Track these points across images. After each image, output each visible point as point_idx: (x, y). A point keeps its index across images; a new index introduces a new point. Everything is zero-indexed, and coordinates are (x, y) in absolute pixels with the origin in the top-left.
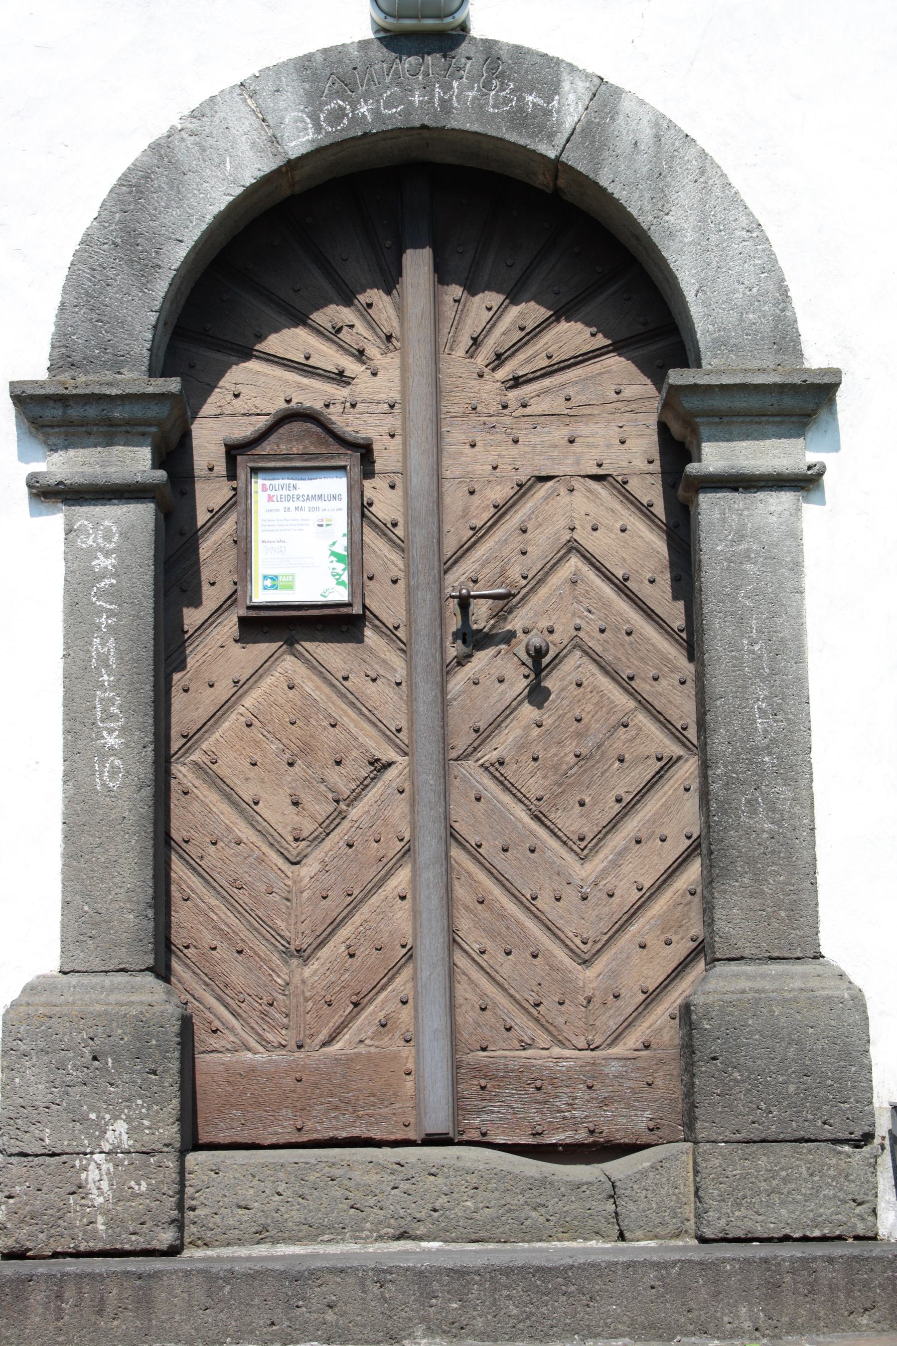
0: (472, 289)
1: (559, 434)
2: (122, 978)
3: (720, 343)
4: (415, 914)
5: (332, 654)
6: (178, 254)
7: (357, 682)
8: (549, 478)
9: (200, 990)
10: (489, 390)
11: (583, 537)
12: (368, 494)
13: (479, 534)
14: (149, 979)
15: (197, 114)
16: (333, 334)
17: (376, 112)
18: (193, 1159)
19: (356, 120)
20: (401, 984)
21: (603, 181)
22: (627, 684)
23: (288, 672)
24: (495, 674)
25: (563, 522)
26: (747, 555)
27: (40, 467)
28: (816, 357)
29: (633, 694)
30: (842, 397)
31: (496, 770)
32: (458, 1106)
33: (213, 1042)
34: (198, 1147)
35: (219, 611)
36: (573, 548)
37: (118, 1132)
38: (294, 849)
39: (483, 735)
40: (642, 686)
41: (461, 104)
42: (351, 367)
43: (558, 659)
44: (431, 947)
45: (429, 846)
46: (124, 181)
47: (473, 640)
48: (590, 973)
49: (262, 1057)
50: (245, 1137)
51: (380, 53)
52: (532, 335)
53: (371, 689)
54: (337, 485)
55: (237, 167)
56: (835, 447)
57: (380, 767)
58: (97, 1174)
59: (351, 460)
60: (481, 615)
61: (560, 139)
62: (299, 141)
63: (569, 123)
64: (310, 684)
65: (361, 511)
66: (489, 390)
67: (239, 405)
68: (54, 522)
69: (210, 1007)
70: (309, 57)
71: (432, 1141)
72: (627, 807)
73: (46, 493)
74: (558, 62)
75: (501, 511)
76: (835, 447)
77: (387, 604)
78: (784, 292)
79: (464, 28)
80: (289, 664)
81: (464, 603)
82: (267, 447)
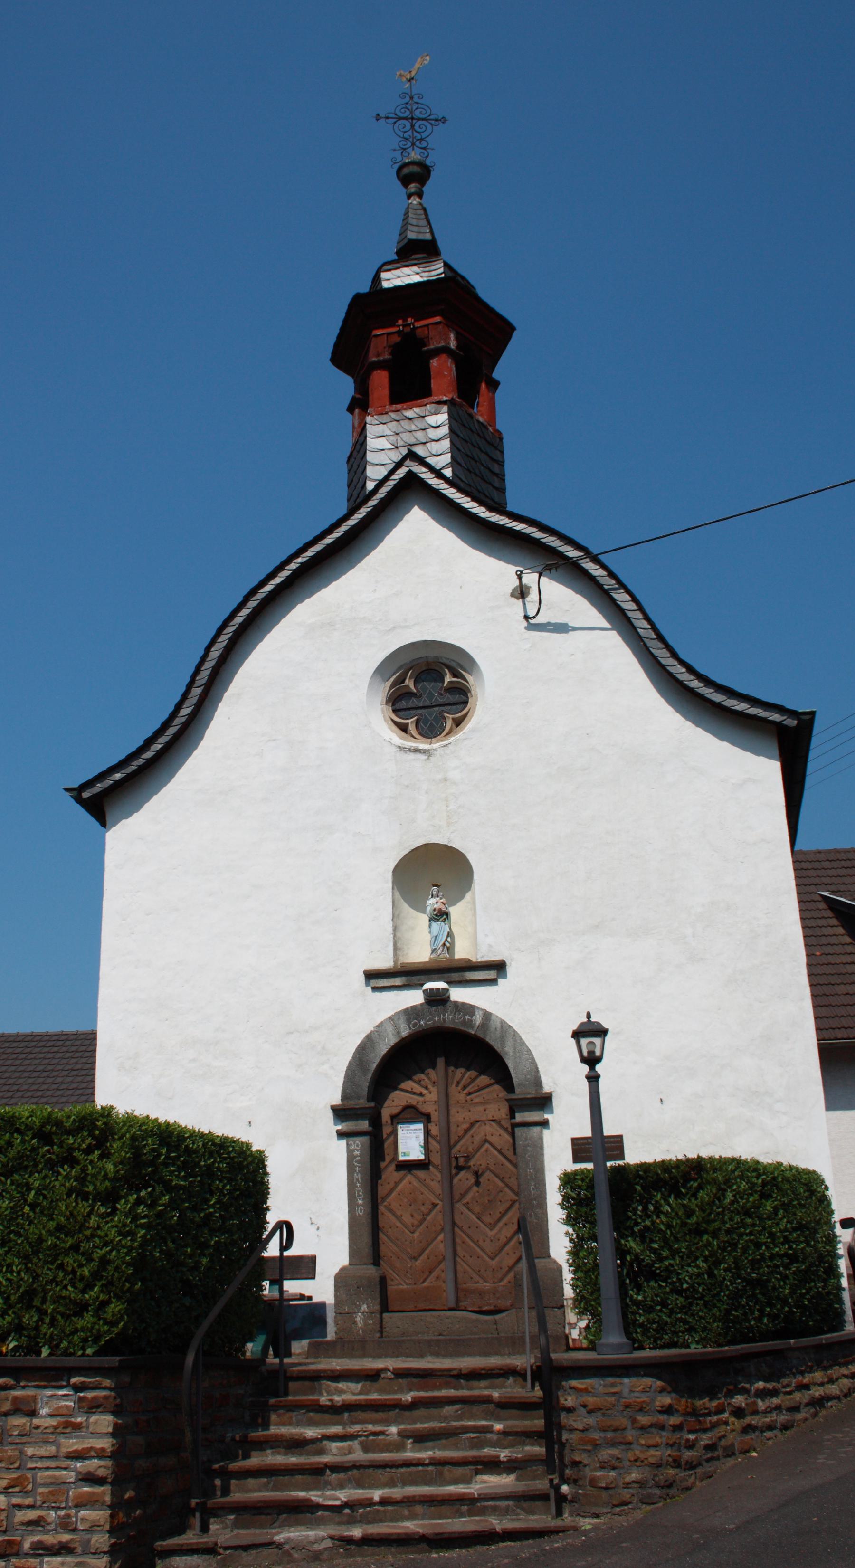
0: (457, 1067)
1: (481, 1108)
2: (365, 1266)
3: (519, 1085)
4: (445, 1246)
5: (421, 1174)
6: (374, 1066)
7: (428, 1181)
8: (478, 1121)
9: (388, 1269)
10: (462, 1097)
11: (489, 1138)
12: (430, 1127)
13: (460, 1138)
14: (372, 1267)
15: (378, 1026)
16: (419, 1082)
17: (425, 1023)
18: (385, 1315)
19: (421, 1026)
20: (442, 1266)
21: (488, 1039)
22: (502, 1179)
23: (409, 1180)
24: (464, 1179)
25: (483, 1134)
26: (528, 1145)
27: (339, 1127)
28: (547, 1089)
29: (503, 1182)
30: (554, 1100)
31: (466, 1205)
32: (457, 1300)
33: (392, 1283)
34: (388, 1311)
35: (390, 1162)
36: (486, 1141)
37: (364, 1307)
38: (412, 1229)
39: (463, 1195)
40: (506, 1180)
41: (449, 1019)
42: (425, 1091)
43: (483, 1173)
44: (449, 1255)
45: (448, 1228)
46: (359, 1046)
47: (459, 1168)
48: (494, 1262)
49: (405, 1287)
50: (401, 1309)
51: (426, 1006)
52: (473, 1080)
53: (432, 1183)
54: (421, 1126)
55: (389, 1040)
56: (552, 1112)
57: (435, 1205)
58: (359, 1318)
59: (424, 1119)
60: (461, 1161)
61: (476, 1028)
62: (405, 1032)
63: (478, 1023)
64: (415, 1183)
65: (427, 1133)
66: (462, 1097)
67: (394, 1104)
68: (343, 1143)
69: (390, 1273)
70: (407, 1009)
71: (451, 1309)
72: (503, 1215)
73: (341, 1135)
74: (474, 1006)
75: (466, 1131)
76: (552, 1112)
77: (436, 1159)
78: (537, 1068)
79: (449, 997)
80: (409, 1177)
81: (457, 1158)
82: (401, 1116)
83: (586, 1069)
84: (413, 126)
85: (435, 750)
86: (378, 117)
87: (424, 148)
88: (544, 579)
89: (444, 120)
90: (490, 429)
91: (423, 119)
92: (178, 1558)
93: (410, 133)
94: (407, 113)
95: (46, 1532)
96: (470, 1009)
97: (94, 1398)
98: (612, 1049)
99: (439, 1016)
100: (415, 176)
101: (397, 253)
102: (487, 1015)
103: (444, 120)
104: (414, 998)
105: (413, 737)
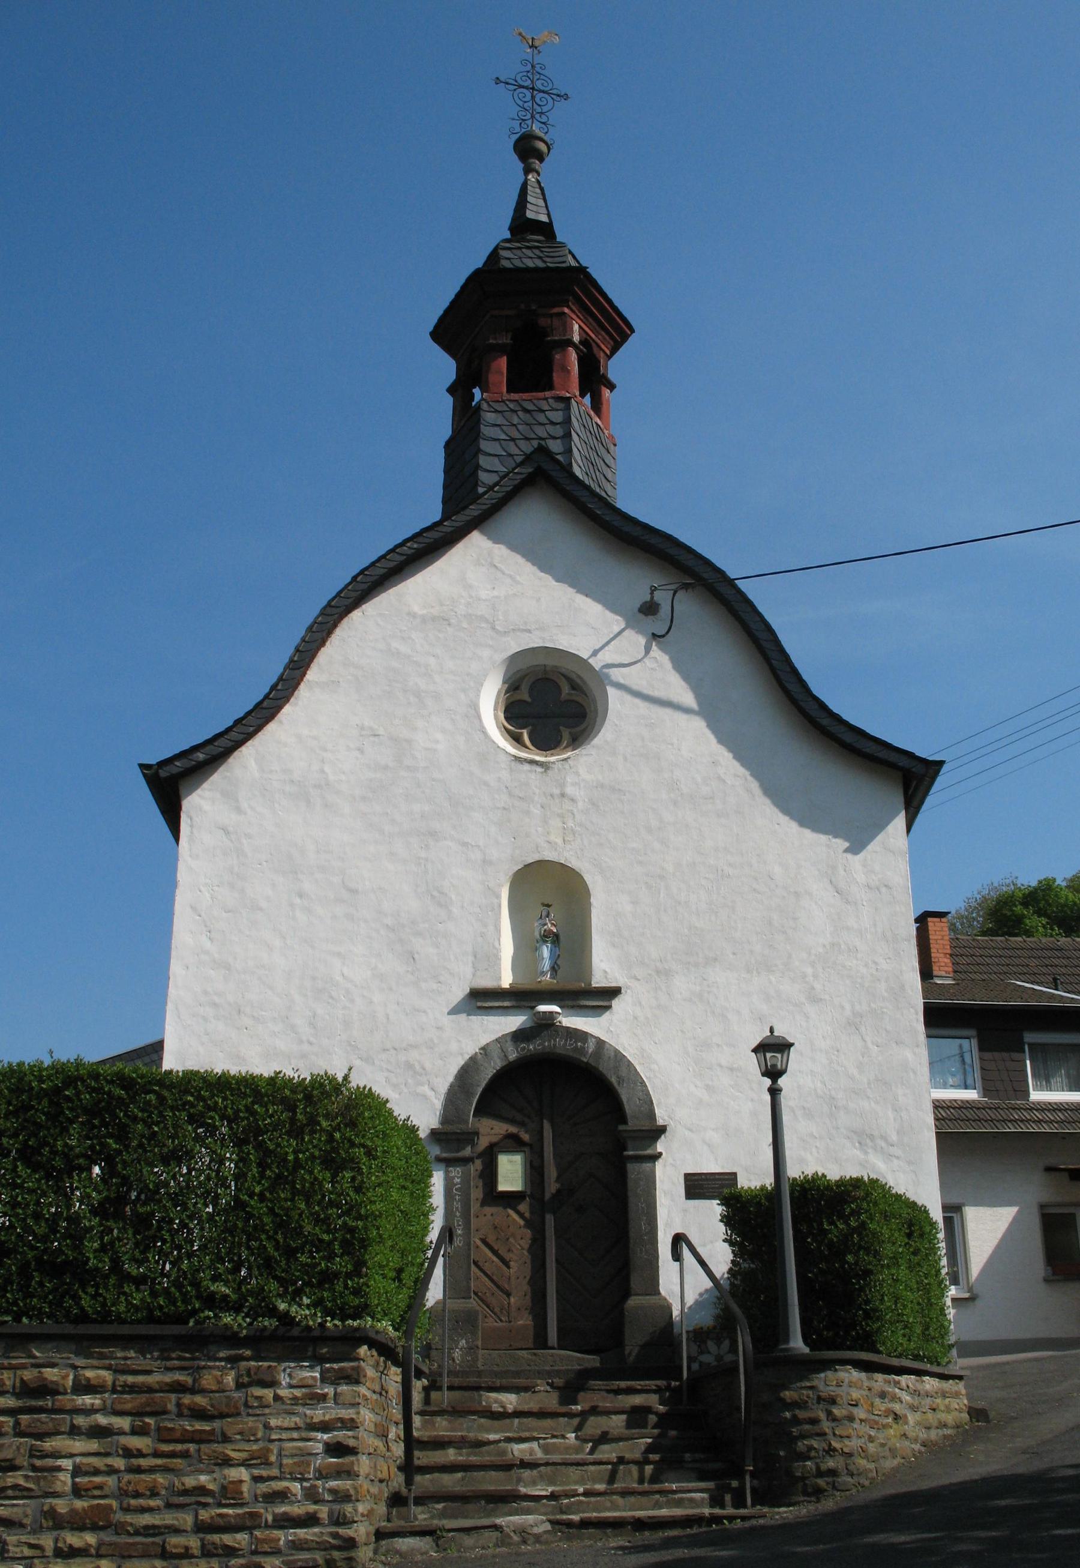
28: (660, 1122)
41: (560, 1045)
62: (513, 1056)
63: (590, 1050)
83: (768, 1082)
84: (533, 97)
85: (553, 763)
86: (498, 81)
87: (544, 123)
88: (680, 595)
89: (566, 97)
90: (606, 432)
91: (523, 87)
92: (401, 1540)
93: (530, 104)
94: (528, 83)
95: (292, 1503)
96: (583, 1036)
97: (341, 1369)
98: (795, 1060)
99: (550, 1041)
100: (528, 150)
101: (511, 229)
102: (600, 1043)
103: (566, 97)
104: (515, 1022)
105: (527, 747)
